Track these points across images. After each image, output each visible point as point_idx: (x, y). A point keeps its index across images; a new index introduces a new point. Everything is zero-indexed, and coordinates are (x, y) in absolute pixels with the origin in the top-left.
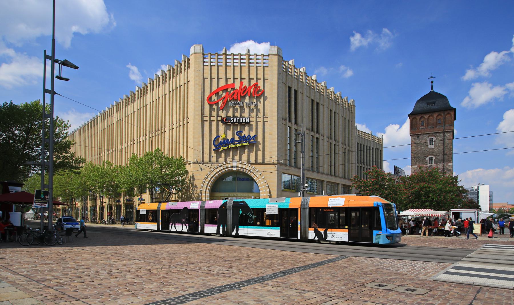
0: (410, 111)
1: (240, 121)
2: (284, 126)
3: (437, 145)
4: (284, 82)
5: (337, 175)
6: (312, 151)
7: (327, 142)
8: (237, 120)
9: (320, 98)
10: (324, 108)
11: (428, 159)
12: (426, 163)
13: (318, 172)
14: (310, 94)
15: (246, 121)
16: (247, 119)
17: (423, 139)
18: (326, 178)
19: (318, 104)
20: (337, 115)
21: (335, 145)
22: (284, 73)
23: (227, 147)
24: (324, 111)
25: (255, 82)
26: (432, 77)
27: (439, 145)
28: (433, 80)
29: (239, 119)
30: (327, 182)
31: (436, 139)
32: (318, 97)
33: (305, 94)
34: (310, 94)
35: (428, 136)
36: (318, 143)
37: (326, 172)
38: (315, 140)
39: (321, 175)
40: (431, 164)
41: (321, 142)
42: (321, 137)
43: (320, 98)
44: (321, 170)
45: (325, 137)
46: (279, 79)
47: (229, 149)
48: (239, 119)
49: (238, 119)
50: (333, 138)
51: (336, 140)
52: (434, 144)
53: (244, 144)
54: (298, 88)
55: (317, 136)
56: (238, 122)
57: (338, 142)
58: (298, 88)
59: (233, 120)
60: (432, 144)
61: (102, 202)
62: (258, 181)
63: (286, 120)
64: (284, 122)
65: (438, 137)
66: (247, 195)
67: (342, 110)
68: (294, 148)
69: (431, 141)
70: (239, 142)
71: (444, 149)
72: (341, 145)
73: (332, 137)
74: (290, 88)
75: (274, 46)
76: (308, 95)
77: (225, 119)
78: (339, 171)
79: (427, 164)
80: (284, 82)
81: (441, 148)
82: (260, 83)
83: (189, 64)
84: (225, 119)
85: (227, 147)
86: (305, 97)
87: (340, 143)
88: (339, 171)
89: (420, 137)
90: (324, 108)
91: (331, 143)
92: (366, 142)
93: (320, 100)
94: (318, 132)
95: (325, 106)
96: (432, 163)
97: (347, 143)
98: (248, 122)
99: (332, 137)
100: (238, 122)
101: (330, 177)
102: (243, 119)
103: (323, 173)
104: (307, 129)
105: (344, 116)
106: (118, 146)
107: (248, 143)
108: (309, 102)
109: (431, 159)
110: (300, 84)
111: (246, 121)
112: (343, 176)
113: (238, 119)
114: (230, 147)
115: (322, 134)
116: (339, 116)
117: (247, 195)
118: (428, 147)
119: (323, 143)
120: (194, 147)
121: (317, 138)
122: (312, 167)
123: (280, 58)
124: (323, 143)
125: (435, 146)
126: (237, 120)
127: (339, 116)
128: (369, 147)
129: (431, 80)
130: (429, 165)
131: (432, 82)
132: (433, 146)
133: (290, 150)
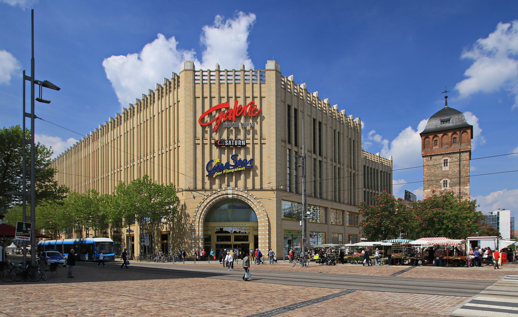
1: (235, 144)
2: (283, 148)
3: (453, 166)
5: (342, 201)
6: (315, 176)
7: (347, 137)
8: (232, 142)
9: (322, 117)
10: (326, 128)
11: (442, 182)
12: (440, 186)
13: (321, 198)
15: (241, 143)
16: (242, 141)
19: (320, 123)
20: (341, 136)
21: (339, 168)
23: (221, 172)
25: (251, 101)
26: (446, 92)
27: (454, 167)
28: (447, 94)
29: (234, 142)
32: (320, 116)
36: (320, 166)
38: (318, 163)
40: (445, 188)
41: (324, 165)
42: (324, 160)
43: (322, 117)
44: (324, 196)
46: (277, 97)
47: (224, 175)
48: (234, 142)
49: (233, 141)
50: (337, 161)
53: (240, 169)
54: (298, 106)
55: (319, 158)
56: (233, 144)
57: (343, 165)
58: (298, 106)
59: (228, 143)
60: (447, 166)
61: (88, 234)
62: (255, 209)
63: (285, 142)
64: (283, 144)
65: (453, 157)
66: (244, 224)
67: (347, 130)
69: (446, 162)
70: (235, 167)
71: (460, 171)
72: (346, 168)
73: (337, 159)
74: (289, 107)
75: (271, 61)
76: (310, 114)
77: (218, 142)
78: (343, 197)
81: (457, 169)
82: (257, 102)
83: (178, 82)
84: (218, 142)
85: (221, 172)
86: (306, 116)
87: (345, 166)
88: (343, 197)
90: (326, 128)
91: (335, 166)
93: (322, 119)
94: (320, 154)
96: (446, 187)
97: (352, 165)
98: (244, 144)
99: (337, 159)
100: (233, 144)
101: (335, 204)
102: (239, 141)
104: (308, 151)
105: (350, 137)
106: (103, 173)
107: (244, 167)
108: (311, 121)
109: (445, 183)
110: (300, 102)
111: (241, 143)
112: (348, 202)
113: (233, 141)
114: (225, 172)
115: (325, 156)
116: (343, 137)
118: (442, 169)
119: (327, 166)
121: (320, 161)
124: (327, 166)
125: (449, 168)
126: (232, 142)
127: (343, 137)
128: (377, 170)
129: (445, 95)
130: (443, 189)
131: (446, 97)
132: (447, 168)
133: (290, 174)
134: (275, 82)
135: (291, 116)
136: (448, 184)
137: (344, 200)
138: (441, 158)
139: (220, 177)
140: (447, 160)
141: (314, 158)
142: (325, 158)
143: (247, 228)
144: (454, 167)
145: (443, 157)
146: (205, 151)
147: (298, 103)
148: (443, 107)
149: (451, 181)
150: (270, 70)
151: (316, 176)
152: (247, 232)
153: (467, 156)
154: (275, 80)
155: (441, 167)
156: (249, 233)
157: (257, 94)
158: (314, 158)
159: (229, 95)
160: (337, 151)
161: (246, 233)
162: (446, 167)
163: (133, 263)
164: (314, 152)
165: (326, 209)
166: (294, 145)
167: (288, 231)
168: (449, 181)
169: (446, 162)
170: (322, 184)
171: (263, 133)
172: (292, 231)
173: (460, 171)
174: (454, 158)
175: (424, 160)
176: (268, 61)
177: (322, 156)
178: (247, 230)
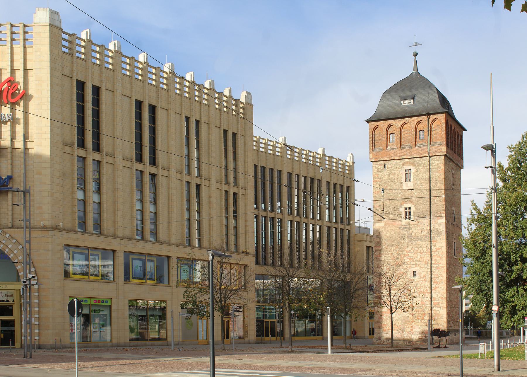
0: (370, 114)
2: (128, 170)
3: (419, 182)
4: (67, 72)
11: (402, 210)
14: (132, 91)
17: (393, 170)
18: (175, 253)
22: (68, 57)
24: (168, 121)
25: (9, 76)
26: (416, 44)
27: (421, 183)
28: (417, 49)
30: (179, 258)
33: (119, 91)
34: (132, 91)
35: (403, 165)
36: (198, 195)
37: (175, 239)
39: (162, 246)
41: (161, 181)
45: (173, 172)
46: (51, 70)
51: (201, 177)
52: (412, 179)
54: (101, 82)
57: (208, 179)
58: (101, 82)
62: (12, 255)
64: (68, 149)
65: (418, 166)
68: (232, 222)
69: (408, 173)
71: (430, 190)
75: (42, 9)
79: (401, 221)
80: (67, 72)
82: (19, 77)
87: (213, 182)
89: (389, 164)
92: (334, 176)
95: (212, 126)
103: (169, 243)
104: (125, 159)
115: (165, 165)
117: (4, 286)
118: (402, 186)
120: (374, 207)
121: (198, 186)
122: (227, 243)
123: (54, 30)
125: (414, 185)
131: (416, 55)
134: (49, 46)
135: (85, 100)
136: (412, 214)
139: (364, 336)
141: (186, 181)
142: (206, 179)
143: (9, 293)
144: (421, 183)
147: (101, 76)
148: (406, 72)
149: (416, 209)
150: (41, 24)
151: (191, 211)
152: (11, 300)
154: (49, 41)
155: (402, 183)
156: (14, 301)
157: (18, 64)
158: (186, 181)
159: (15, 65)
161: (8, 301)
162: (408, 182)
164: (227, 183)
166: (148, 164)
167: (97, 300)
169: (408, 173)
170: (101, 205)
171: (30, 131)
172: (89, 300)
173: (430, 190)
174: (420, 167)
176: (37, 9)
177: (158, 166)
178: (10, 296)
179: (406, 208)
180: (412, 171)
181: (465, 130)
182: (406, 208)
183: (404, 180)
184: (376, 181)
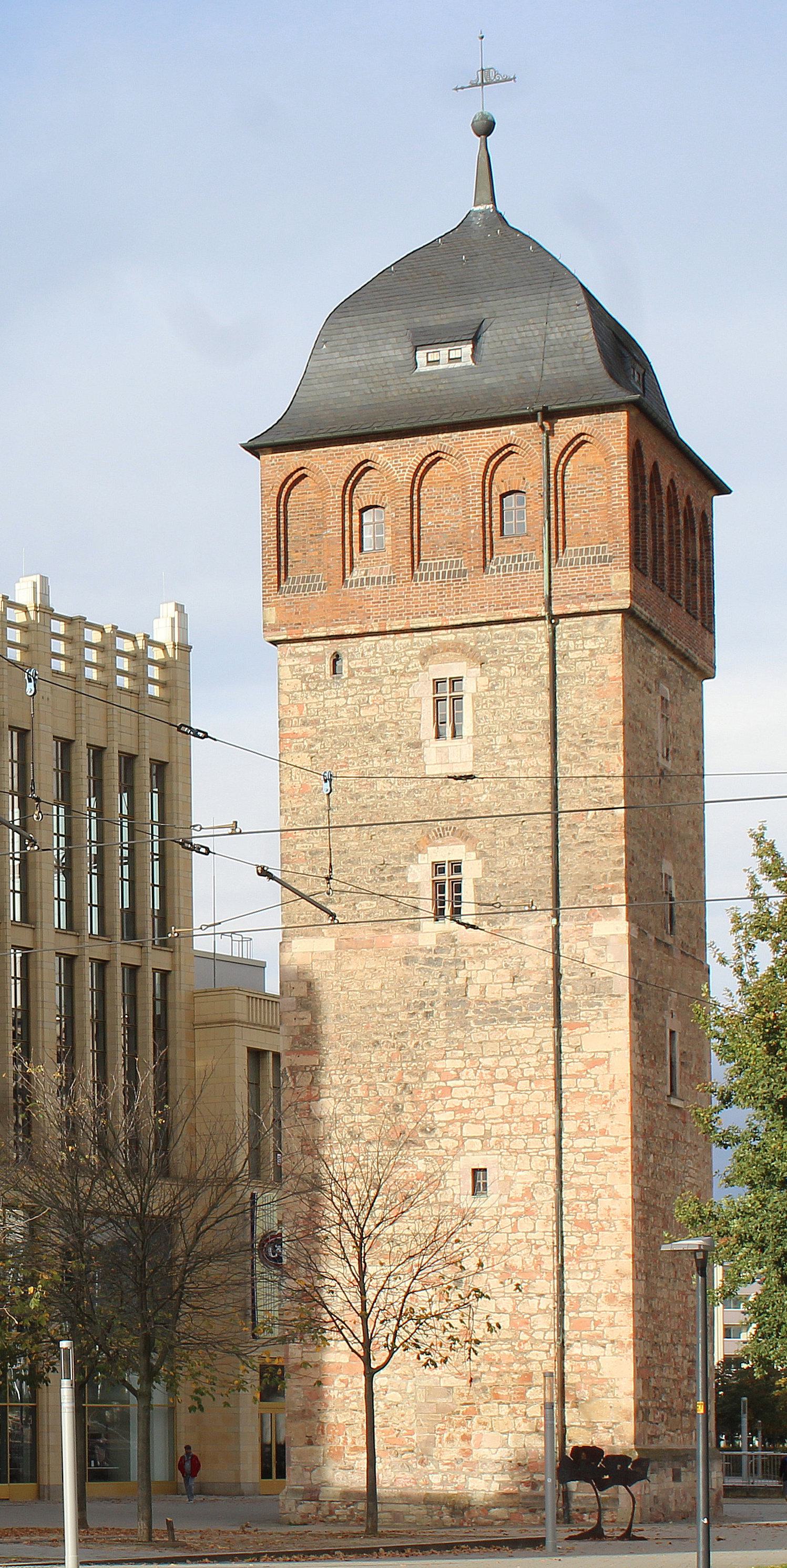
3: (500, 740)
26: (485, 79)
27: (511, 745)
31: (484, 680)
52: (467, 729)
65: (499, 663)
71: (554, 778)
79: (415, 928)
125: (476, 756)
131: (486, 128)
137: (268, 1004)
138: (415, 664)
140: (455, 681)
144: (511, 745)
145: (425, 658)
146: (583, 418)
149: (488, 870)
153: (604, 658)
155: (418, 745)
160: (560, 529)
162: (448, 742)
163: (719, 1311)
165: (194, 1026)
168: (471, 873)
173: (554, 778)
174: (505, 671)
175: (286, 673)
179: (438, 868)
180: (468, 688)
181: (723, 489)
182: (438, 868)
183: (428, 729)
184: (294, 736)
